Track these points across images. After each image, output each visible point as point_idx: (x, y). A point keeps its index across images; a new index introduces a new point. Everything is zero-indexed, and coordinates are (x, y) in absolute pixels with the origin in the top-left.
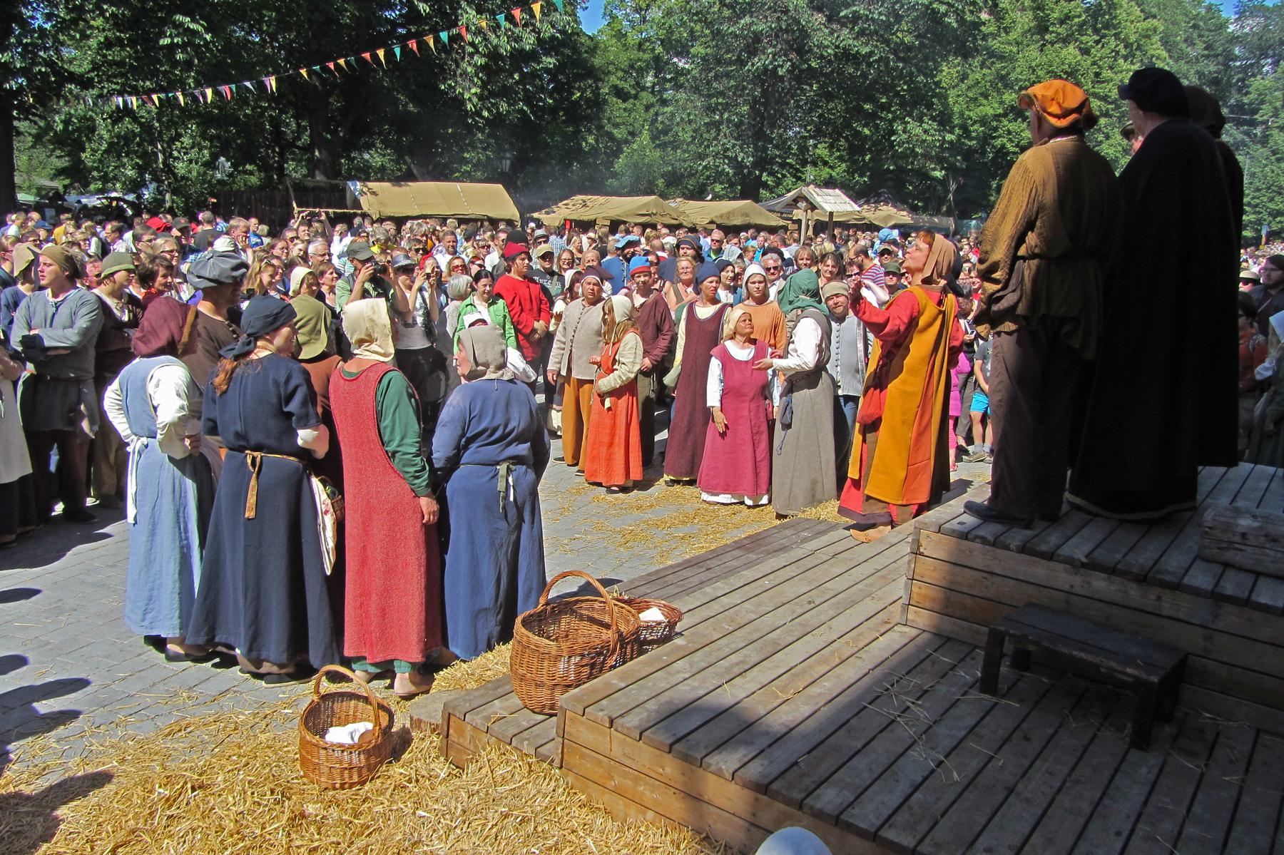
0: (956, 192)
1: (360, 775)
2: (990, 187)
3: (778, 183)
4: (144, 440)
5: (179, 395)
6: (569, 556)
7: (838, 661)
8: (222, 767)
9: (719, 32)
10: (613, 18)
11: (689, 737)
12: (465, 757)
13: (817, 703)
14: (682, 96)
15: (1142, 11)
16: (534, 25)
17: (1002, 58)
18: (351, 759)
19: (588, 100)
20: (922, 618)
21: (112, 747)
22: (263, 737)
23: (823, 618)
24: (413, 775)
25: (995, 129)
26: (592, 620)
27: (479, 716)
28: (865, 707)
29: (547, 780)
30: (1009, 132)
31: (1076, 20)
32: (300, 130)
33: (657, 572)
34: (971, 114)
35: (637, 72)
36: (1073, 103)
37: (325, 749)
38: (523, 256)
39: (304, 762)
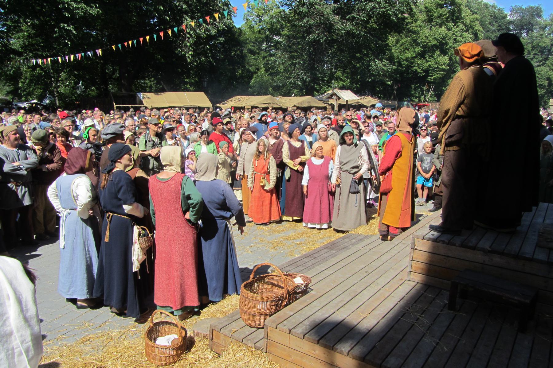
0: (397, 90)
1: (174, 359)
2: (412, 88)
3: (321, 88)
4: (69, 211)
5: (88, 191)
6: (251, 254)
7: (384, 298)
8: (110, 358)
9: (294, 25)
10: (248, 20)
11: (326, 336)
12: (221, 349)
13: (378, 318)
14: (279, 53)
15: (471, 11)
16: (215, 24)
17: (414, 33)
18: (170, 352)
19: (238, 55)
20: (418, 278)
21: (57, 350)
22: (126, 343)
23: (373, 279)
24: (198, 358)
25: (412, 63)
26: (272, 284)
27: (227, 330)
28: (400, 319)
29: (260, 358)
30: (418, 64)
31: (445, 17)
32: (114, 72)
33: (293, 260)
34: (402, 57)
35: (259, 43)
36: (475, 52)
37: (158, 348)
38: (220, 124)
39: (148, 354)
